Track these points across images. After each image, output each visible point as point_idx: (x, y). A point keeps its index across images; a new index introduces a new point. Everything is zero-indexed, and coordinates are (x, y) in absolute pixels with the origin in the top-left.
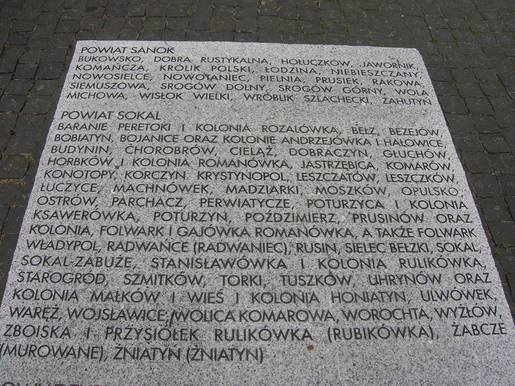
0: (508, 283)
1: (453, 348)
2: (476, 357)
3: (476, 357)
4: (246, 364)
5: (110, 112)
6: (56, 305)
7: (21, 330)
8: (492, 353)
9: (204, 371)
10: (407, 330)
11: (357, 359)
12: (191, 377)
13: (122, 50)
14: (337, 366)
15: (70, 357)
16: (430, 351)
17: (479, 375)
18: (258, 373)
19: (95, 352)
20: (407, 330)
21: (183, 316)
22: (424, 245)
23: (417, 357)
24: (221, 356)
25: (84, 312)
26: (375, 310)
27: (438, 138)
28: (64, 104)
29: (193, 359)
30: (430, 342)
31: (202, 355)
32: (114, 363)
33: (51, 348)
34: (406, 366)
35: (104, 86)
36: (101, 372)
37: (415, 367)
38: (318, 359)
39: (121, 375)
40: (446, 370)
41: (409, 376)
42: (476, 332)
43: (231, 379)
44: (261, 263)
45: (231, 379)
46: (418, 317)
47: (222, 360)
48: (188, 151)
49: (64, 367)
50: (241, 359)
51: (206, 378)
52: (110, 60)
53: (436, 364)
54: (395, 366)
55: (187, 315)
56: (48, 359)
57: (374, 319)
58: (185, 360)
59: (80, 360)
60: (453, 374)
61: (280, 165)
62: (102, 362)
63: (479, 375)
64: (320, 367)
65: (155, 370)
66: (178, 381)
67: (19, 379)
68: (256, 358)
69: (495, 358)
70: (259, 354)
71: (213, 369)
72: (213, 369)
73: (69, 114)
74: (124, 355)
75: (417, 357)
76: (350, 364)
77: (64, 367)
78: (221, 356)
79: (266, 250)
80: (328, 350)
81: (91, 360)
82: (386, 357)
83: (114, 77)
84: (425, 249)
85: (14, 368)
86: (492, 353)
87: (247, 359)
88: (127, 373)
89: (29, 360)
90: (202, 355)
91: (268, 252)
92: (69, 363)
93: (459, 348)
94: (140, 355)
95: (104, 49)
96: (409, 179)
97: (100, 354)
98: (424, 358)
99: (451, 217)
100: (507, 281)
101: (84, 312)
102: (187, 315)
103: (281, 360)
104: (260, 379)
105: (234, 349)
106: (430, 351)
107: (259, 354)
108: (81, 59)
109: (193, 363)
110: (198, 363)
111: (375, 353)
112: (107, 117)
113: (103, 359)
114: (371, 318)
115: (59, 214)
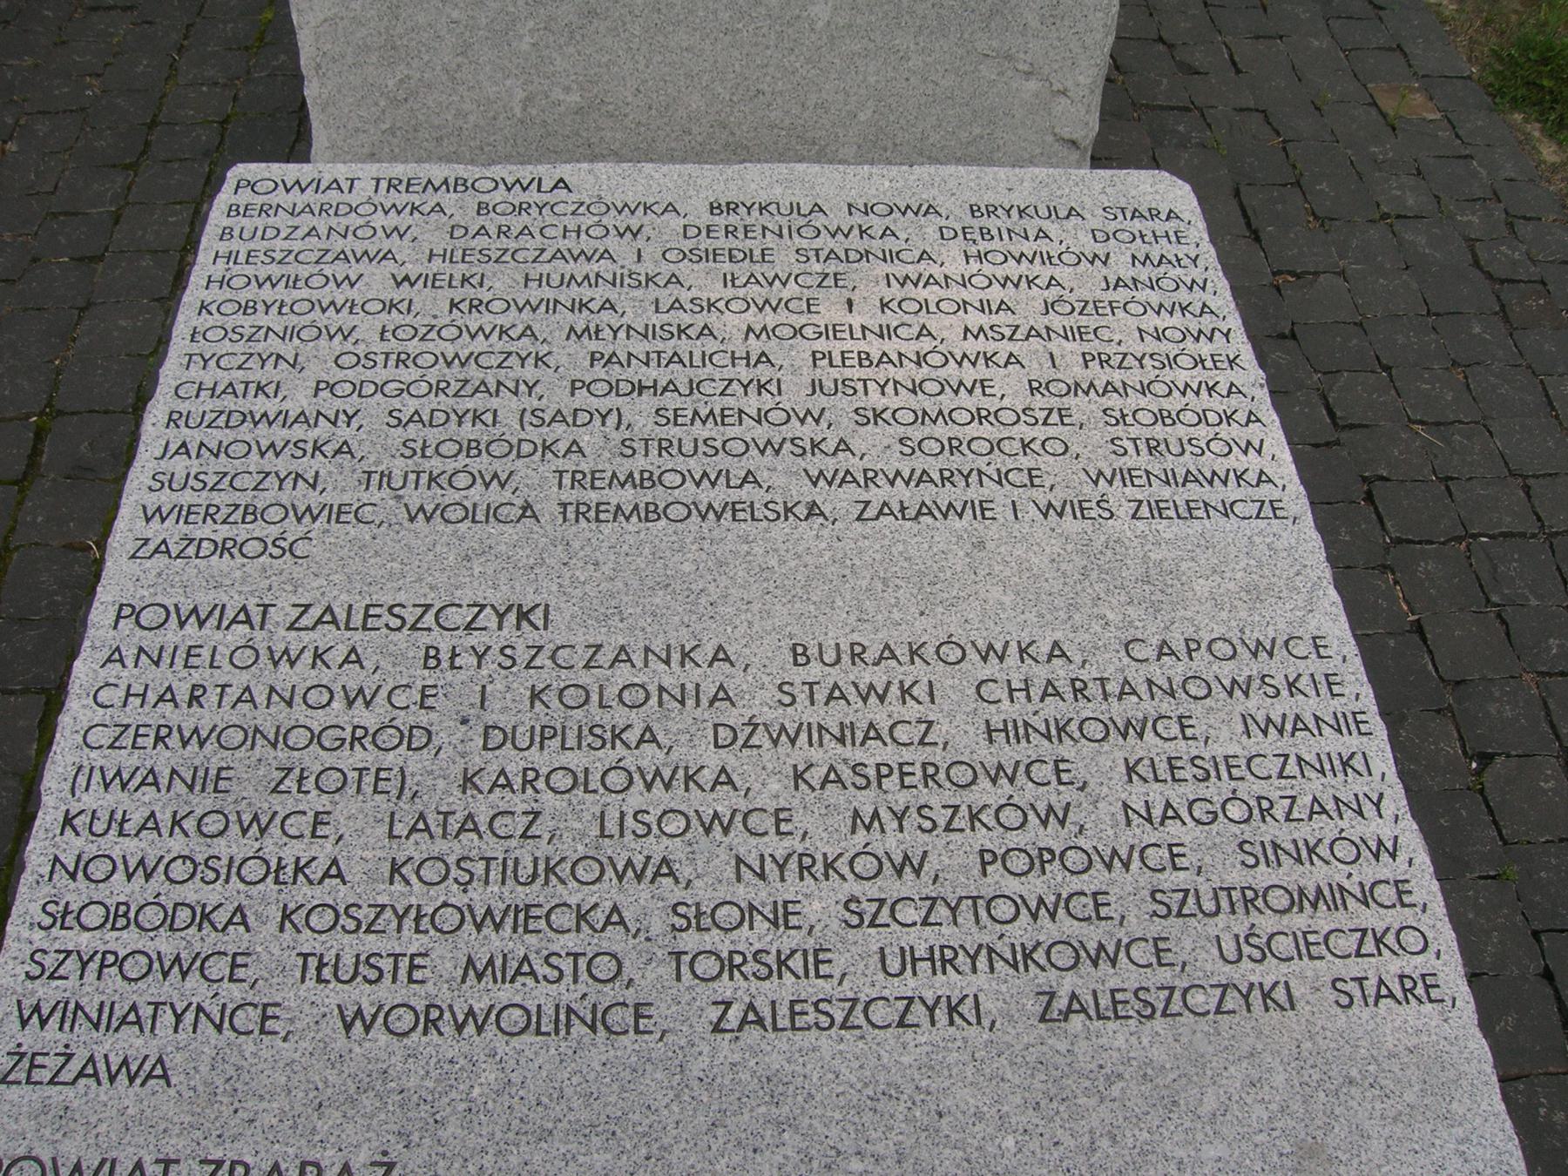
6: (67, 1046)
7: (132, 915)
10: (1232, 473)
13: (345, 186)
19: (824, 962)
20: (1232, 473)
21: (363, 1020)
22: (798, 956)
25: (387, 1014)
26: (1250, 888)
35: (192, 482)
46: (1371, 1001)
48: (541, 784)
52: (288, 191)
55: (375, 1017)
57: (731, 978)
83: (230, 335)
84: (1361, 768)
91: (818, 976)
95: (396, 228)
96: (884, 916)
99: (1265, 804)
101: (387, 1014)
102: (375, 1017)
114: (726, 975)
115: (102, 1067)
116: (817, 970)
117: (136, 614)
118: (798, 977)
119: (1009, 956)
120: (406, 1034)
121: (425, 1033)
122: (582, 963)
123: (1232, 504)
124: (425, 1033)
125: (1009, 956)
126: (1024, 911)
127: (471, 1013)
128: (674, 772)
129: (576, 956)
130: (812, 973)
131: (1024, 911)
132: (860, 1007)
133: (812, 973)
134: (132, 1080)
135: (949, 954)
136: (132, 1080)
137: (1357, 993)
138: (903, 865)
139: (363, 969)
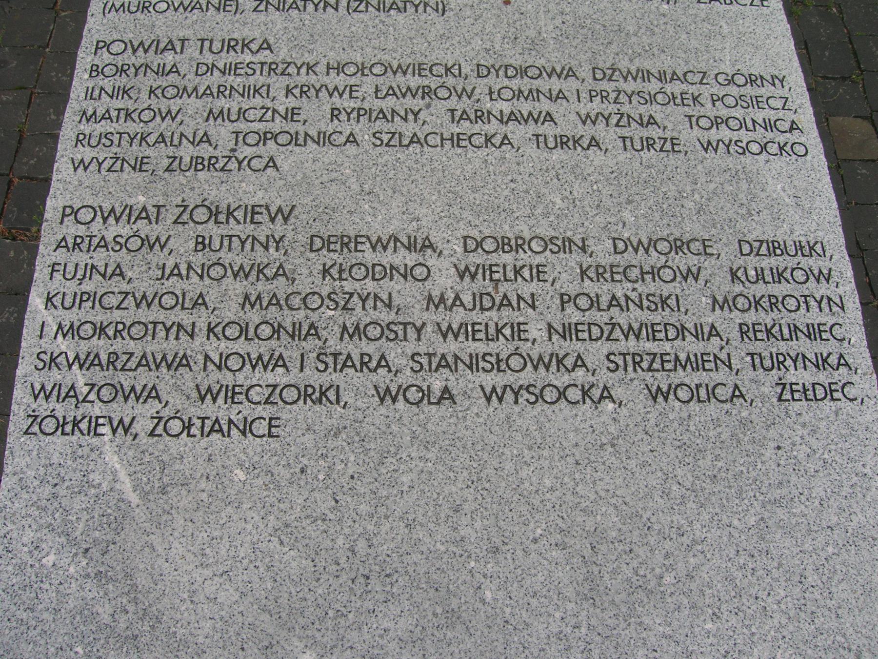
0: (808, 53)
1: (696, 15)
2: (725, 27)
3: (725, 27)
4: (423, 17)
5: (158, 207)
8: (747, 25)
9: (370, 23)
11: (568, 17)
12: (353, 29)
14: (542, 23)
15: (196, 11)
16: (664, 15)
17: (727, 45)
18: (438, 26)
19: (258, 213)
23: (646, 20)
24: (391, 8)
27: (785, 92)
28: (67, 187)
29: (355, 11)
30: (666, 7)
31: (367, 7)
32: (254, 15)
33: (119, 387)
34: (632, 29)
36: (237, 25)
37: (643, 31)
38: (517, 15)
39: (263, 28)
40: (684, 36)
41: (634, 39)
42: (778, 252)
43: (404, 32)
44: (456, 331)
45: (404, 32)
47: (392, 12)
49: (189, 21)
50: (417, 11)
51: (371, 30)
53: (671, 31)
54: (617, 28)
56: (167, 14)
57: (305, 403)
58: (345, 12)
59: (209, 14)
60: (693, 42)
61: (570, 367)
62: (238, 15)
63: (727, 45)
64: (518, 23)
65: (307, 22)
66: (336, 33)
67: (131, 35)
68: (437, 10)
69: (751, 30)
70: (441, 6)
71: (381, 21)
72: (381, 21)
73: (108, 46)
74: (266, 8)
75: (646, 20)
76: (557, 23)
77: (189, 21)
78: (391, 8)
79: (574, 337)
80: (530, 6)
81: (222, 14)
82: (606, 17)
85: (123, 25)
86: (747, 25)
87: (425, 11)
88: (270, 26)
89: (143, 16)
90: (367, 7)
92: (195, 18)
93: (703, 15)
94: (287, 7)
97: (234, 8)
98: (655, 23)
100: (806, 48)
103: (468, 13)
104: (441, 32)
105: (410, 323)
106: (664, 15)
107: (441, 6)
108: (90, 95)
109: (355, 15)
110: (361, 15)
111: (591, 12)
112: (178, 50)
113: (239, 11)
116: (233, 398)
117: (108, 46)
118: (507, 340)
119: (814, 361)
120: (177, 436)
121: (228, 52)
122: (694, 120)
123: (714, 387)
124: (228, 52)
125: (814, 361)
126: (529, 364)
127: (409, 89)
128: (477, 269)
129: (624, 355)
130: (516, 338)
131: (529, 364)
132: (605, 335)
133: (516, 338)
134: (138, 399)
135: (781, 358)
136: (138, 399)
137: (621, 363)
138: (464, 272)
139: (104, 140)
